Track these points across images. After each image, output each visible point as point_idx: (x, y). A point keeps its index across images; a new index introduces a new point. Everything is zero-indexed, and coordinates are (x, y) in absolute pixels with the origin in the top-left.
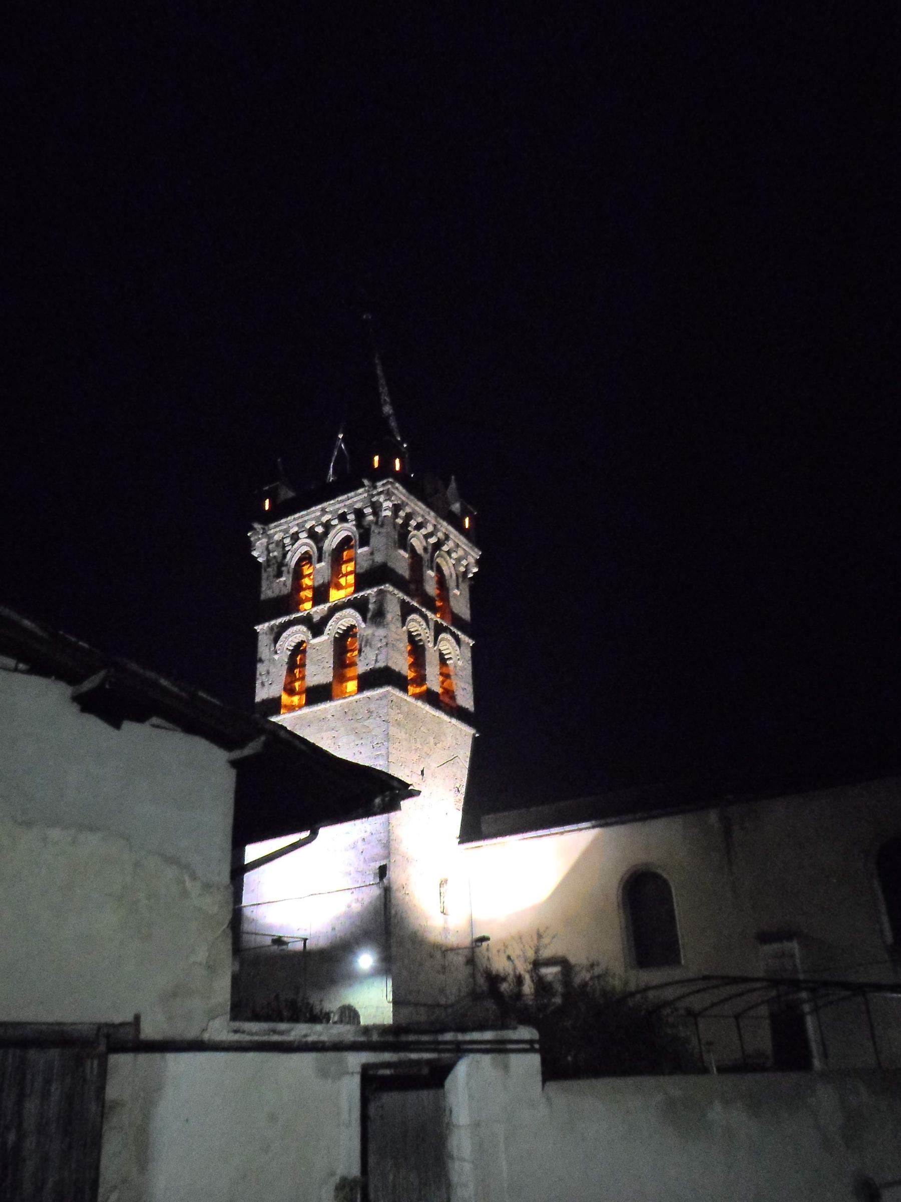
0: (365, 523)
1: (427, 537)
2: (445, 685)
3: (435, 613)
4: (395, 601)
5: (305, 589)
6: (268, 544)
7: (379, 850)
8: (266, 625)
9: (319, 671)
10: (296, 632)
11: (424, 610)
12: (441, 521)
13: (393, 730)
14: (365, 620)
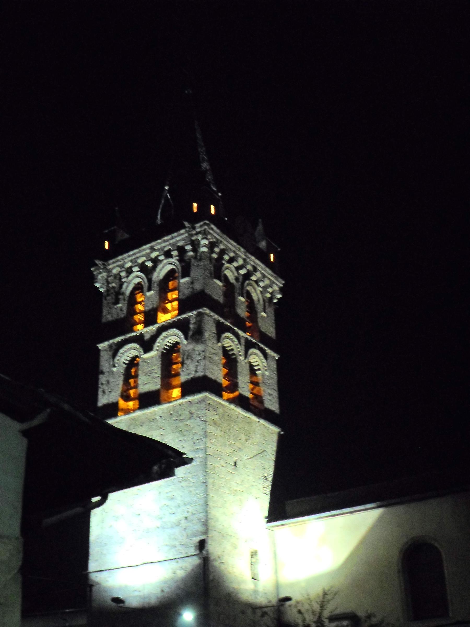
0: (186, 258)
1: (238, 269)
3: (245, 332)
6: (108, 276)
7: (199, 527)
9: (149, 382)
10: (131, 349)
12: (250, 256)
14: (186, 338)
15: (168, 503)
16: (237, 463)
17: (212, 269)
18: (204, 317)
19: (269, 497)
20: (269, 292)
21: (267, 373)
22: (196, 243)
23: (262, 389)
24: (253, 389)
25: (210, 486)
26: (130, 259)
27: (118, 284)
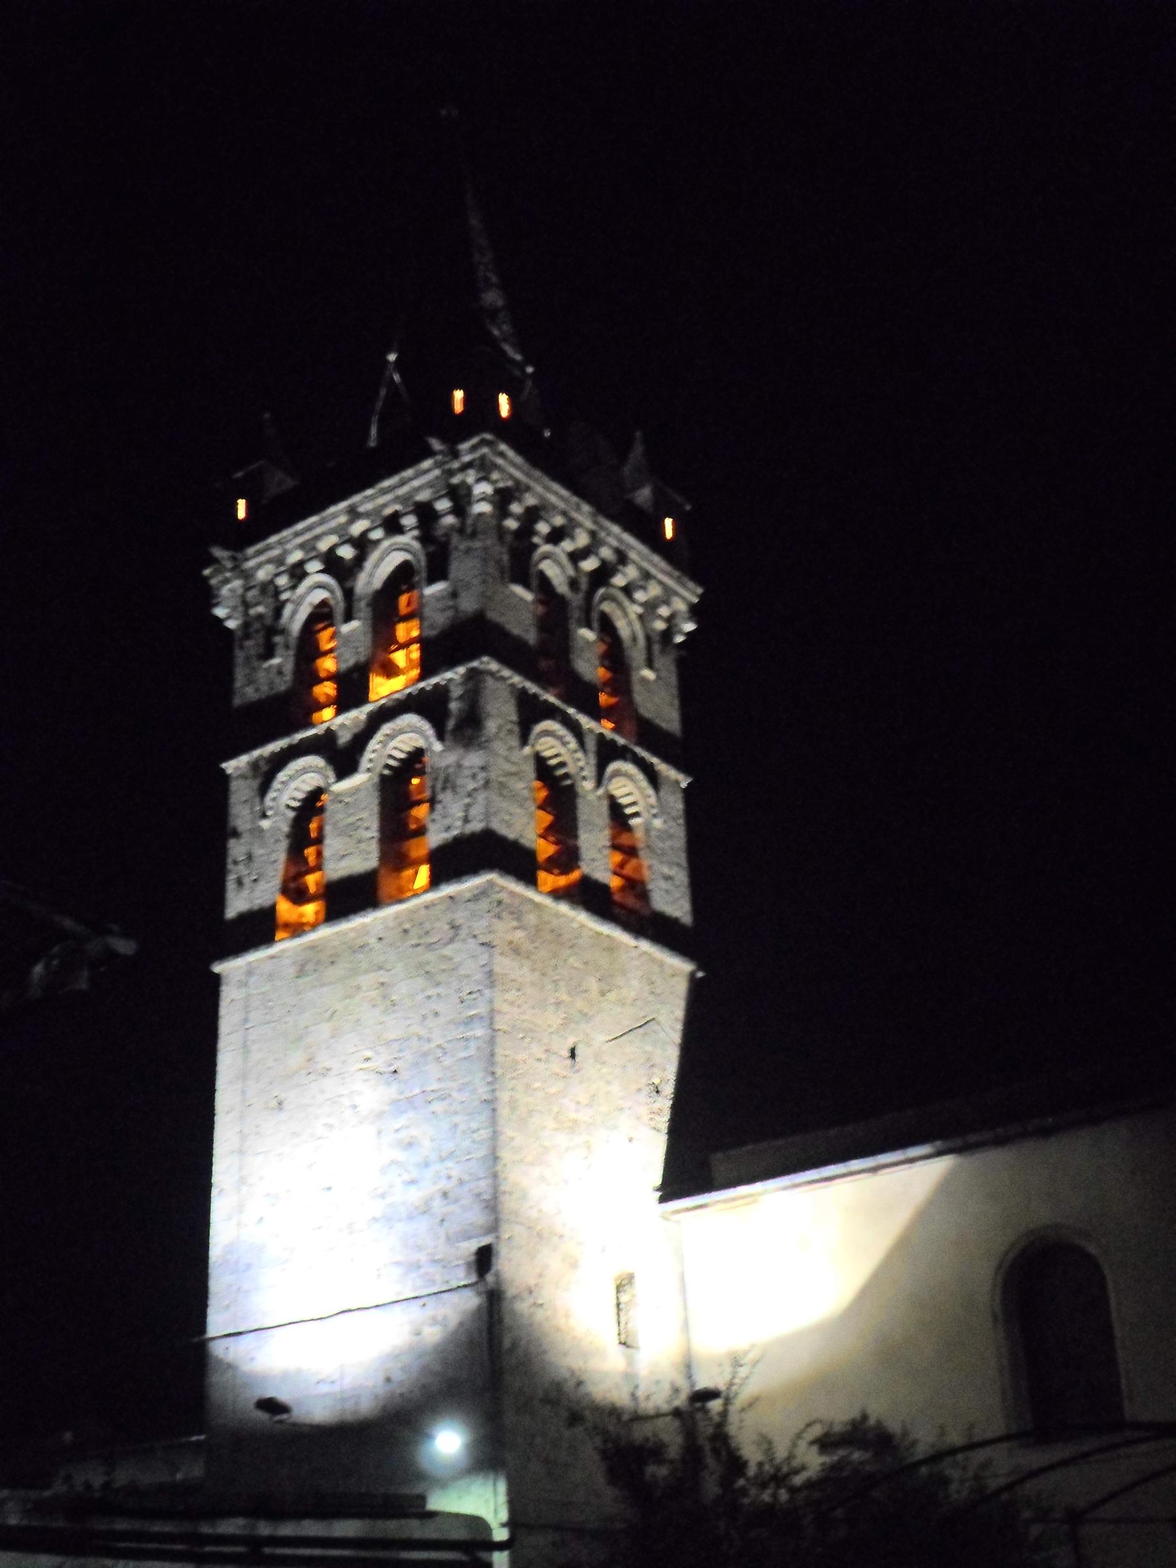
0: (439, 532)
1: (576, 557)
2: (628, 870)
4: (505, 693)
5: (320, 681)
6: (248, 589)
7: (477, 1216)
8: (243, 760)
9: (349, 851)
10: (305, 771)
11: (571, 711)
14: (441, 737)
15: (401, 1156)
16: (577, 1052)
17: (506, 558)
18: (484, 681)
19: (666, 1137)
20: (660, 617)
21: (658, 823)
22: (463, 492)
24: (622, 865)
25: (504, 1111)
26: (300, 540)
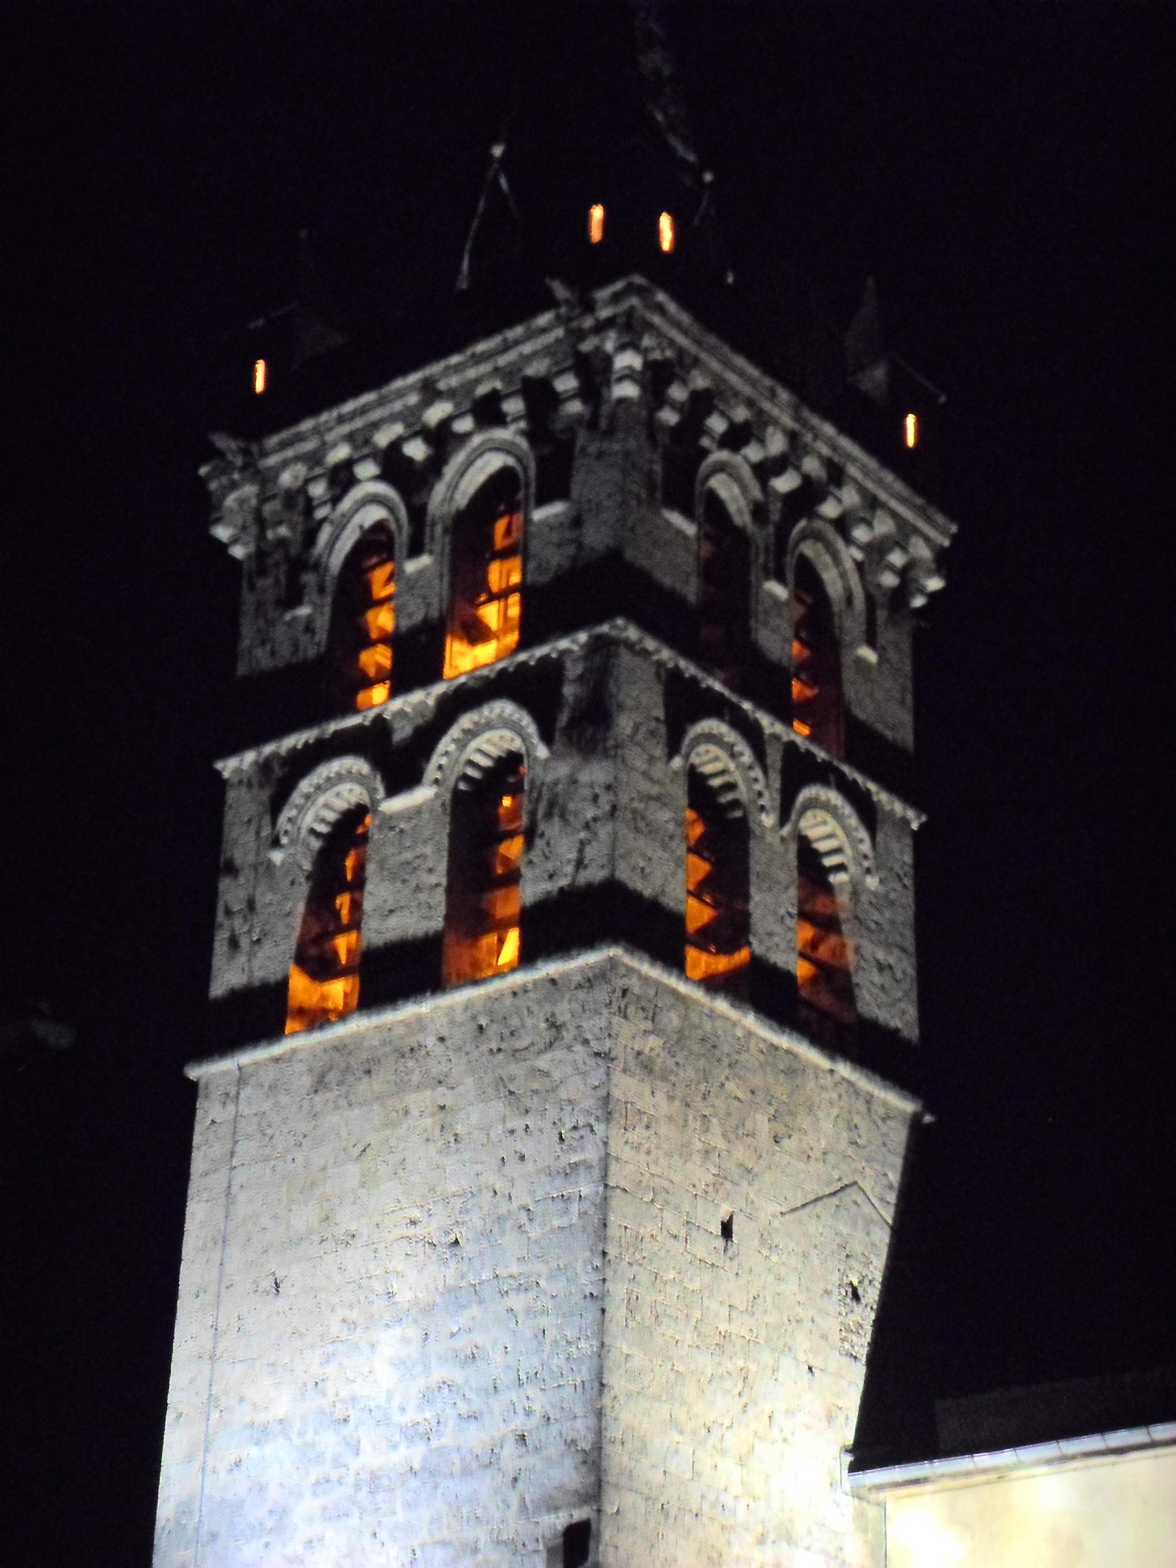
1: (765, 470)
2: (823, 952)
3: (787, 721)
4: (646, 672)
6: (263, 499)
7: (568, 1475)
9: (401, 903)
10: (340, 778)
11: (747, 706)
12: (815, 421)
13: (626, 1086)
14: (547, 736)
15: (457, 1375)
17: (657, 468)
20: (891, 568)
23: (850, 943)
24: (814, 944)
25: (617, 1312)
26: (346, 429)
27: (300, 528)
